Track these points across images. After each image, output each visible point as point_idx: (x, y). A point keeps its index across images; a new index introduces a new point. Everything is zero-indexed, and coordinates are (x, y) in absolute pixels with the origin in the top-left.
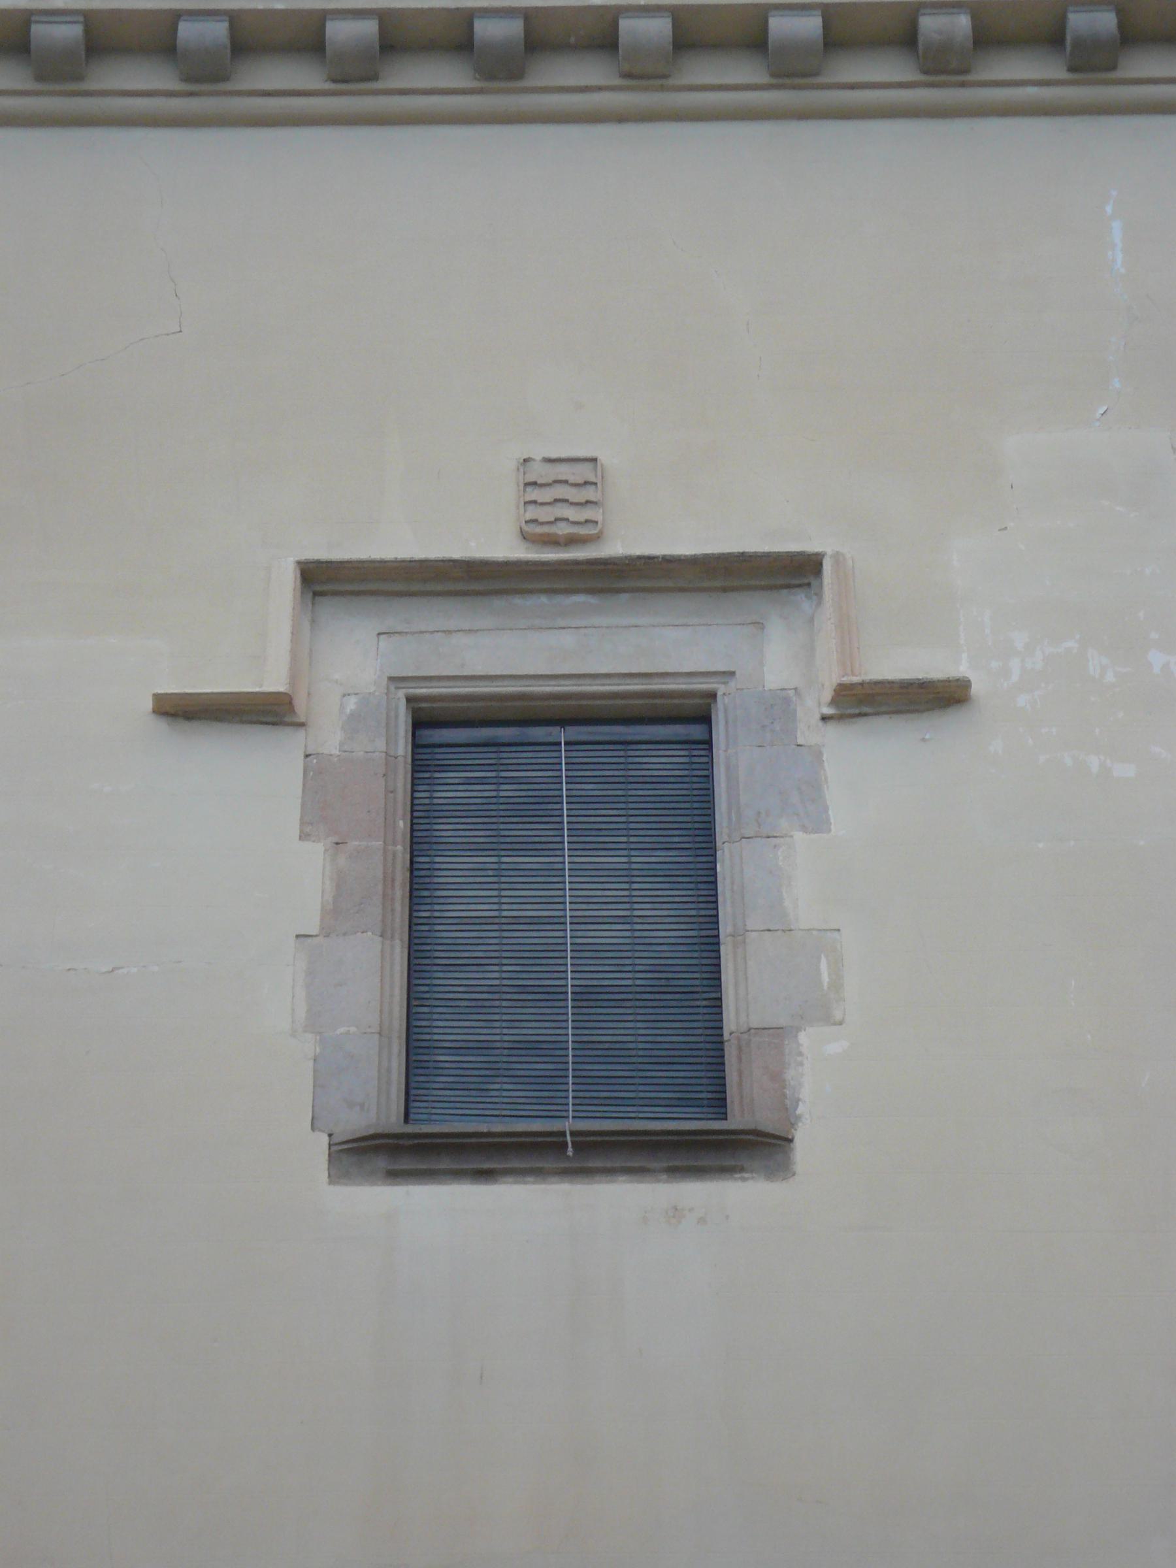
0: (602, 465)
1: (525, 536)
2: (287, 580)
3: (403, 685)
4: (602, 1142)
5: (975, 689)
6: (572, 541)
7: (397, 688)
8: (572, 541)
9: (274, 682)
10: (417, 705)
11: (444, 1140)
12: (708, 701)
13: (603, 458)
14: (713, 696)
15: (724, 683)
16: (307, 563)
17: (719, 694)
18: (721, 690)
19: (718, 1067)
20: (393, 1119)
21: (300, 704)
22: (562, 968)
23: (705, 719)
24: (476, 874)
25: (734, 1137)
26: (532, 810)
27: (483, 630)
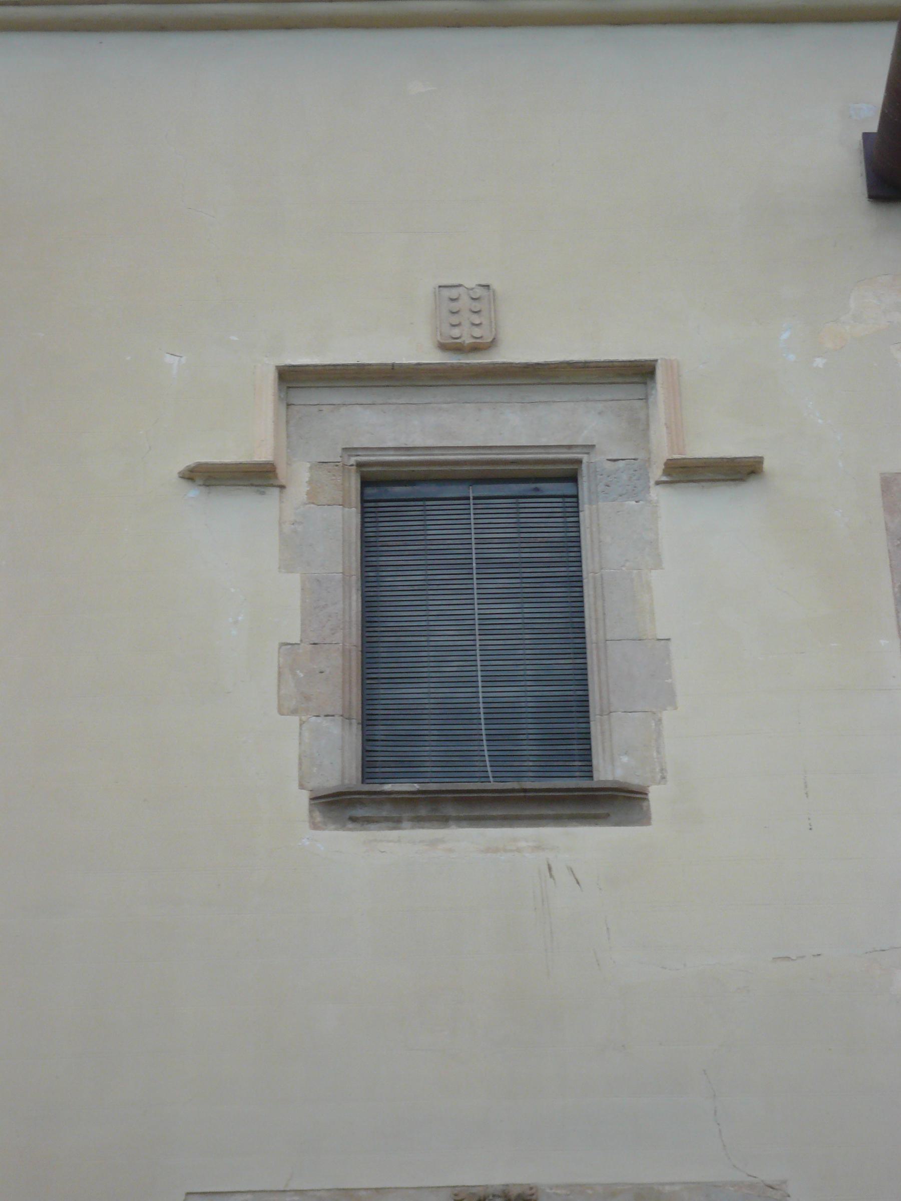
0: (494, 291)
1: (443, 347)
2: (271, 377)
3: (354, 453)
4: (402, 799)
5: (766, 465)
6: (475, 348)
7: (350, 456)
8: (475, 348)
9: (262, 455)
10: (364, 469)
11: (466, 795)
12: (575, 467)
13: (495, 285)
14: (579, 462)
15: (588, 453)
16: (290, 366)
17: (584, 461)
18: (585, 458)
19: (585, 741)
20: (354, 782)
21: (282, 471)
22: (474, 668)
23: (573, 478)
24: (519, 656)
25: (597, 793)
26: (395, 506)
27: (628, 640)
